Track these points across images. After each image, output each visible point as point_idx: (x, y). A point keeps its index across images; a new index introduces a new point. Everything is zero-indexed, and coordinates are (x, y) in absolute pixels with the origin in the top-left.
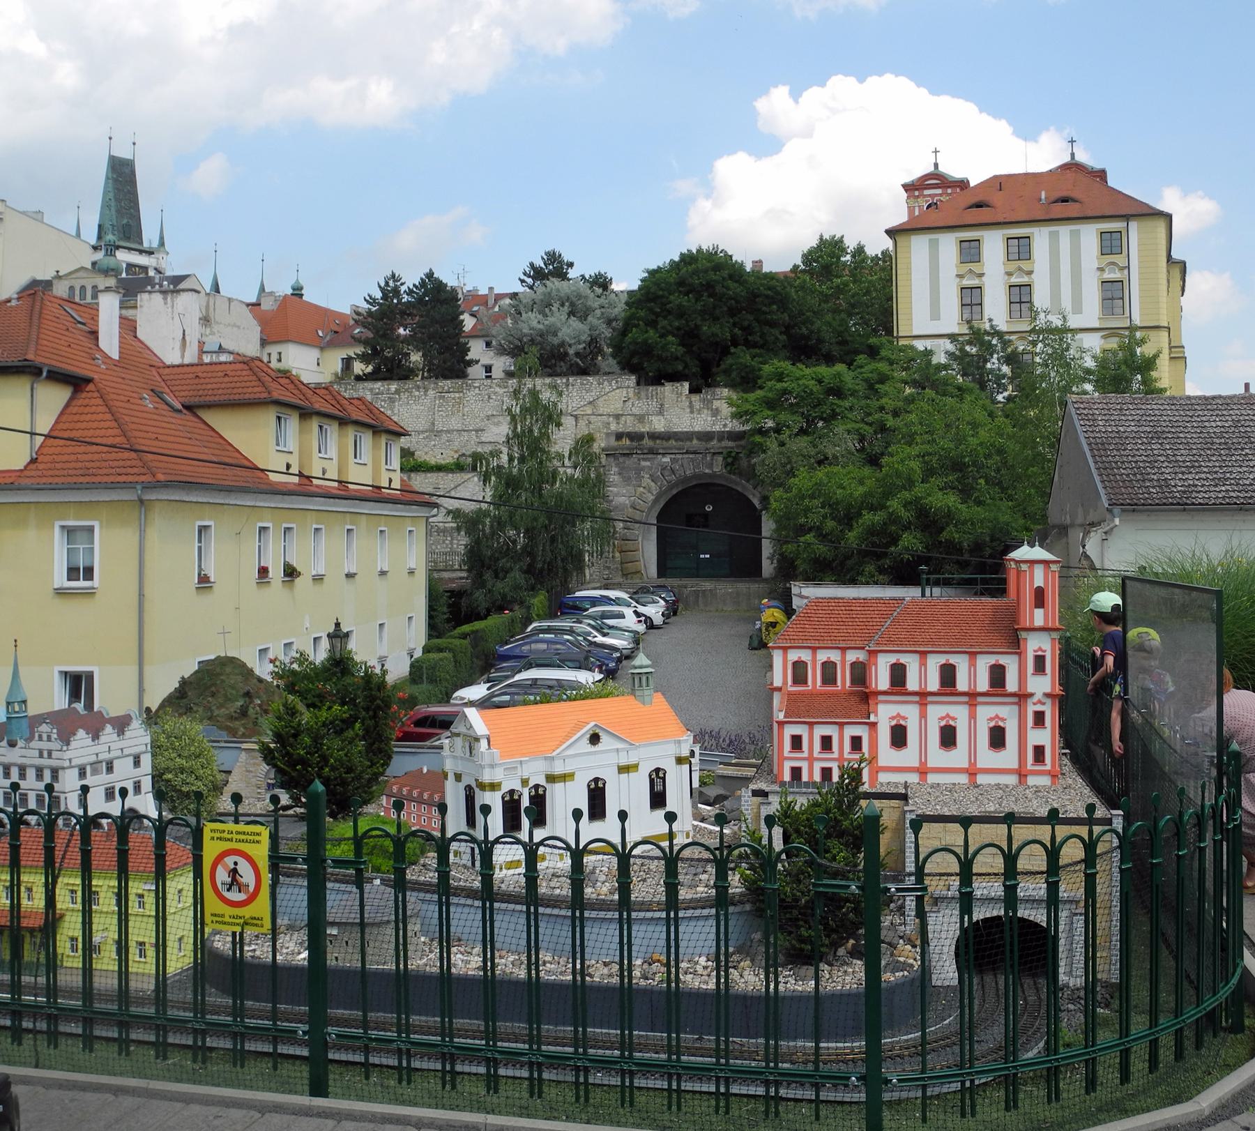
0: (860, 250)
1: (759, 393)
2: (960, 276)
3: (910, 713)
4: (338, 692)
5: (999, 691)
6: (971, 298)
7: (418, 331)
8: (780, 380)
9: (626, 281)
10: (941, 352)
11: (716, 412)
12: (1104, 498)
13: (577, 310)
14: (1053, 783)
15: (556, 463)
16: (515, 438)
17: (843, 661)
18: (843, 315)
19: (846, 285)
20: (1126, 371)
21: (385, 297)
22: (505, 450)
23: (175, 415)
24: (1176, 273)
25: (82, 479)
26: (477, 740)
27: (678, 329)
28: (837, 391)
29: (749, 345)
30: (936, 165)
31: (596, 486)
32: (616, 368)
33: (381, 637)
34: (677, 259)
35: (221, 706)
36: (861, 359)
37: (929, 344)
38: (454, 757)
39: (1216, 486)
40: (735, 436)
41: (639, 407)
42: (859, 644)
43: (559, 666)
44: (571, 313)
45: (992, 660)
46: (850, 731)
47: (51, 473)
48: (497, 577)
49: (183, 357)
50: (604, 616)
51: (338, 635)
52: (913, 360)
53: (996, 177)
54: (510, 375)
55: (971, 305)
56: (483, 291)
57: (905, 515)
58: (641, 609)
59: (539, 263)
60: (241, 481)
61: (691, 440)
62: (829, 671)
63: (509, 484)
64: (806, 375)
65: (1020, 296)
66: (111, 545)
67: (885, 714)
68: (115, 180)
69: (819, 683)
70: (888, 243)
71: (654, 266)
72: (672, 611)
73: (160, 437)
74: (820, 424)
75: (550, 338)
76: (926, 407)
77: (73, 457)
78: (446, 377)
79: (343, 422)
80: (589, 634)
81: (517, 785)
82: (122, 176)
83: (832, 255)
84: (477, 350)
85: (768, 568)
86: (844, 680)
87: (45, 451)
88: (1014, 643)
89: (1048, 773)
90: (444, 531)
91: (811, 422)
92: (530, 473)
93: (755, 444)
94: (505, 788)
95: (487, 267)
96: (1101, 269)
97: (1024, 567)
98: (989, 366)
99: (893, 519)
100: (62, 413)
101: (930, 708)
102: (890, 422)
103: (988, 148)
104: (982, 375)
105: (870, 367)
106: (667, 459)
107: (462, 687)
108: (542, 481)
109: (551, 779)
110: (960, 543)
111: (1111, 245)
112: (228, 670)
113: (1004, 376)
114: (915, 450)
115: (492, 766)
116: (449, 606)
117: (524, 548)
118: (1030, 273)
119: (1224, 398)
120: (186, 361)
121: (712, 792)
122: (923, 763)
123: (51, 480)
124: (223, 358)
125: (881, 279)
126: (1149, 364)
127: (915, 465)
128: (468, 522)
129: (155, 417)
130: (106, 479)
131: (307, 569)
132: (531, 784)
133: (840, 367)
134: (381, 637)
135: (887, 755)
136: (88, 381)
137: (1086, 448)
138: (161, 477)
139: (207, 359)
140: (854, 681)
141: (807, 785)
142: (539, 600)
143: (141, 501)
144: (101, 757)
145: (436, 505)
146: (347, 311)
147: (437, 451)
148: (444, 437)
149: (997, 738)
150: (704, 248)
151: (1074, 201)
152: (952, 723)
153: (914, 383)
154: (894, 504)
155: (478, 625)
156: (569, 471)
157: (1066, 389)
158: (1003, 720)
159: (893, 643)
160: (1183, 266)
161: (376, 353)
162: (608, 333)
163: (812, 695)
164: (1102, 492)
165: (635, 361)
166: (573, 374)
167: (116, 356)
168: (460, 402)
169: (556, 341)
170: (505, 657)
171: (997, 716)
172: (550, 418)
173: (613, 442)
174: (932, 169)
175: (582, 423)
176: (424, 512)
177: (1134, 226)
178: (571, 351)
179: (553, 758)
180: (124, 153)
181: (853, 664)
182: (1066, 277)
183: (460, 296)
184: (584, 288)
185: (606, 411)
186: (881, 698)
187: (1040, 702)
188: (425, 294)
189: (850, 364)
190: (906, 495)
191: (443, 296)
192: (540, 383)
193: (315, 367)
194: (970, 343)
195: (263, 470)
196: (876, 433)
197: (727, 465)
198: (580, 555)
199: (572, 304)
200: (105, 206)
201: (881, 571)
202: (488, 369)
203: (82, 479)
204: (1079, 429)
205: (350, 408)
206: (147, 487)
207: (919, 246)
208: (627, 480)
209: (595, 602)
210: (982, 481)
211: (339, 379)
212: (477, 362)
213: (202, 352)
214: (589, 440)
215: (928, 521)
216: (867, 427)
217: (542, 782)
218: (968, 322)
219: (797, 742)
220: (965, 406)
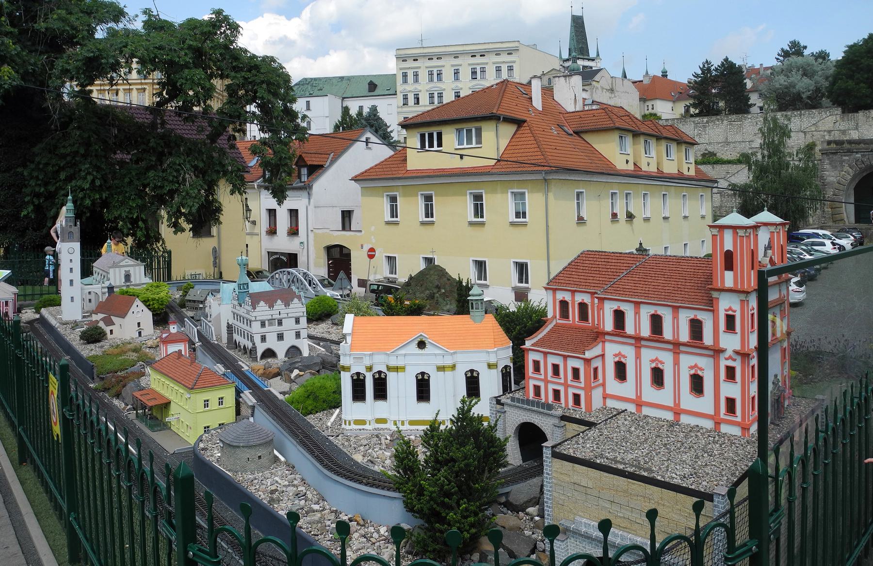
7: (720, 90)
9: (837, 54)
13: (807, 72)
14: (743, 434)
31: (810, 172)
41: (843, 125)
45: (691, 314)
50: (813, 244)
56: (757, 66)
58: (837, 241)
60: (606, 171)
63: (761, 171)
66: (534, 201)
68: (575, 27)
69: (577, 319)
71: (851, 43)
79: (659, 138)
80: (802, 254)
81: (362, 370)
82: (578, 24)
94: (354, 370)
106: (859, 155)
112: (432, 272)
120: (578, 109)
124: (594, 107)
131: (639, 215)
132: (375, 370)
136: (525, 121)
139: (586, 108)
143: (545, 180)
144: (274, 317)
148: (732, 145)
156: (797, 163)
158: (701, 369)
159: (618, 291)
162: (827, 84)
165: (840, 99)
168: (741, 126)
169: (795, 91)
171: (696, 366)
172: (784, 133)
173: (825, 146)
175: (809, 136)
178: (804, 96)
183: (744, 69)
187: (730, 358)
188: (724, 70)
191: (734, 70)
192: (779, 115)
193: (671, 111)
200: (571, 39)
205: (663, 131)
206: (546, 173)
208: (835, 168)
209: (809, 236)
214: (811, 147)
217: (384, 369)
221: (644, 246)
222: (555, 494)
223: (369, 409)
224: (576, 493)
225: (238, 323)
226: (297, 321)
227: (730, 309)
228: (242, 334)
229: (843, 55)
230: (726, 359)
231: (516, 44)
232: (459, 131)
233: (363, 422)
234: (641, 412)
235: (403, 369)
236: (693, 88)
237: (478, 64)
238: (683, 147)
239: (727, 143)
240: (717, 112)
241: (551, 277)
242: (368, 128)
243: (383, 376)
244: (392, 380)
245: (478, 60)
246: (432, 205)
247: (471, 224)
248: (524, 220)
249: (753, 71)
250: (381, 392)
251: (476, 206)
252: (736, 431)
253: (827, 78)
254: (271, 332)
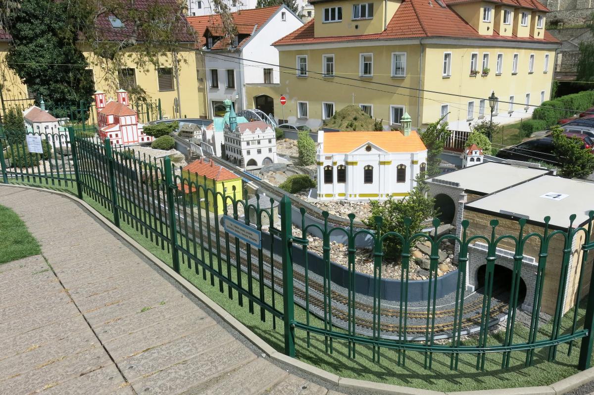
23: (441, 9)
73: (433, 18)
94: (325, 164)
129: (434, 10)
217: (343, 164)
221: (496, 95)
223: (337, 187)
225: (230, 143)
226: (270, 141)
228: (232, 150)
241: (114, 222)
242: (284, 5)
246: (332, 65)
250: (342, 177)
254: (254, 148)
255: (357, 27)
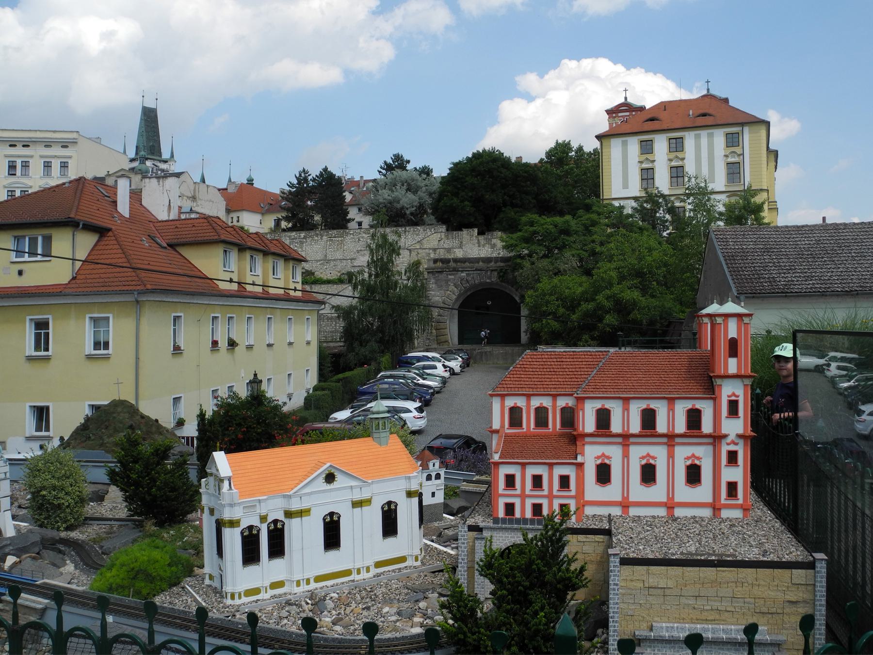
0: (580, 149)
1: (519, 234)
2: (641, 162)
3: (614, 453)
4: (255, 416)
5: (696, 432)
6: (647, 175)
7: (318, 202)
8: (532, 226)
9: (441, 170)
10: (629, 207)
11: (494, 246)
12: (734, 290)
13: (411, 188)
14: (745, 516)
15: (397, 277)
16: (372, 263)
17: (554, 406)
18: (570, 187)
19: (572, 169)
20: (746, 210)
21: (299, 183)
22: (367, 270)
24: (772, 157)
25: (102, 289)
26: (221, 480)
27: (471, 197)
28: (566, 232)
29: (513, 206)
30: (626, 98)
31: (420, 290)
32: (434, 221)
33: (289, 382)
34: (470, 156)
35: (111, 436)
36: (581, 212)
37: (622, 203)
38: (209, 494)
39: (806, 281)
40: (504, 260)
41: (447, 244)
42: (568, 391)
43: (395, 398)
44: (408, 190)
45: (689, 404)
46: (559, 471)
47: (84, 285)
48: (361, 345)
49: (169, 216)
50: (425, 367)
51: (255, 382)
52: (612, 212)
53: (662, 103)
54: (371, 227)
55: (647, 179)
56: (357, 179)
57: (607, 304)
58: (447, 363)
59: (390, 161)
60: (202, 289)
61: (478, 262)
62: (541, 416)
63: (368, 292)
64: (548, 223)
65: (677, 173)
66: (120, 329)
67: (591, 455)
68: (146, 120)
70: (597, 144)
71: (456, 160)
72: (466, 365)
73: (151, 263)
74: (556, 252)
75: (395, 204)
76: (620, 239)
77: (97, 276)
78: (334, 229)
80: (415, 378)
81: (256, 522)
82: (150, 118)
83: (564, 152)
84: (353, 213)
85: (524, 338)
86: (555, 423)
87: (81, 272)
88: (710, 389)
89: (740, 507)
90: (331, 318)
91: (550, 250)
92: (381, 282)
93: (516, 264)
94: (244, 524)
95: (358, 163)
96: (726, 156)
97: (719, 320)
98: (658, 215)
99: (600, 307)
100: (92, 250)
101: (632, 449)
102: (598, 249)
103: (652, 90)
104: (653, 221)
105: (587, 217)
106: (464, 274)
107: (337, 411)
108: (389, 287)
109: (289, 514)
110: (641, 321)
111: (733, 141)
112: (119, 409)
113: (667, 221)
114: (613, 265)
115: (231, 505)
116: (332, 363)
117: (378, 328)
118: (683, 159)
119: (810, 226)
121: (456, 504)
122: (625, 498)
123: (84, 289)
124: (193, 216)
125: (593, 166)
126: (759, 208)
127: (614, 274)
128: (345, 313)
130: (116, 288)
131: (242, 341)
132: (270, 519)
133: (568, 217)
134: (289, 382)
135: (593, 491)
136: (109, 230)
137: (722, 259)
138: (149, 287)
139: (183, 217)
140: (564, 424)
141: (518, 521)
142: (385, 359)
143: (137, 302)
145: (323, 303)
146: (278, 192)
147: (328, 272)
148: (332, 263)
149: (693, 475)
150: (487, 149)
151: (710, 115)
152: (652, 461)
153: (613, 226)
154: (600, 298)
155: (348, 374)
157: (707, 225)
158: (699, 458)
159: (598, 391)
160: (776, 153)
161: (294, 216)
162: (429, 201)
163: (527, 437)
164: (733, 286)
165: (446, 216)
166: (409, 225)
167: (127, 216)
169: (399, 206)
170: (364, 393)
172: (394, 251)
173: (432, 265)
174: (623, 100)
175: (414, 254)
176: (316, 307)
177: (746, 129)
178: (408, 212)
179: (290, 497)
180: (150, 105)
181: (563, 409)
182: (706, 158)
184: (415, 175)
185: (428, 246)
186: (587, 439)
189: (574, 216)
190: (608, 292)
194: (646, 202)
195: (211, 279)
196: (589, 256)
197: (500, 277)
198: (412, 330)
199: (409, 185)
200: (140, 135)
201: (593, 338)
202: (360, 224)
203: (102, 289)
204: (717, 247)
205: (270, 245)
206: (140, 293)
207: (615, 148)
208: (440, 287)
209: (419, 359)
210: (655, 283)
211: (273, 231)
212: (353, 220)
213: (180, 213)
214: (417, 264)
215: (622, 308)
216: (584, 253)
217: (281, 516)
218: (645, 189)
219: (510, 480)
220: (645, 238)
222: (622, 606)
223: (269, 570)
224: (650, 598)
227: (734, 394)
229: (448, 171)
230: (728, 444)
231: (75, 135)
232: (18, 239)
233: (256, 591)
234: (628, 513)
235: (369, 501)
236: (286, 199)
237: (19, 156)
238: (291, 264)
239: (326, 261)
240: (312, 227)
243: (279, 526)
244: (294, 530)
245: (19, 151)
247: (30, 359)
248: (105, 352)
249: (352, 182)
250: (277, 549)
251: (38, 337)
252: (737, 514)
253: (430, 194)
255: (20, 273)
